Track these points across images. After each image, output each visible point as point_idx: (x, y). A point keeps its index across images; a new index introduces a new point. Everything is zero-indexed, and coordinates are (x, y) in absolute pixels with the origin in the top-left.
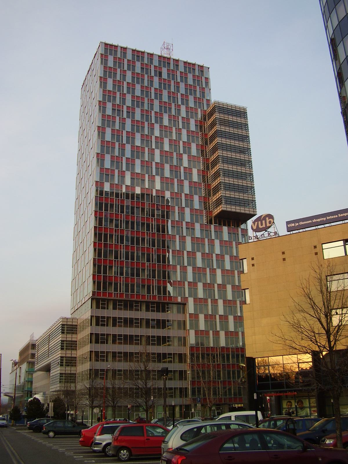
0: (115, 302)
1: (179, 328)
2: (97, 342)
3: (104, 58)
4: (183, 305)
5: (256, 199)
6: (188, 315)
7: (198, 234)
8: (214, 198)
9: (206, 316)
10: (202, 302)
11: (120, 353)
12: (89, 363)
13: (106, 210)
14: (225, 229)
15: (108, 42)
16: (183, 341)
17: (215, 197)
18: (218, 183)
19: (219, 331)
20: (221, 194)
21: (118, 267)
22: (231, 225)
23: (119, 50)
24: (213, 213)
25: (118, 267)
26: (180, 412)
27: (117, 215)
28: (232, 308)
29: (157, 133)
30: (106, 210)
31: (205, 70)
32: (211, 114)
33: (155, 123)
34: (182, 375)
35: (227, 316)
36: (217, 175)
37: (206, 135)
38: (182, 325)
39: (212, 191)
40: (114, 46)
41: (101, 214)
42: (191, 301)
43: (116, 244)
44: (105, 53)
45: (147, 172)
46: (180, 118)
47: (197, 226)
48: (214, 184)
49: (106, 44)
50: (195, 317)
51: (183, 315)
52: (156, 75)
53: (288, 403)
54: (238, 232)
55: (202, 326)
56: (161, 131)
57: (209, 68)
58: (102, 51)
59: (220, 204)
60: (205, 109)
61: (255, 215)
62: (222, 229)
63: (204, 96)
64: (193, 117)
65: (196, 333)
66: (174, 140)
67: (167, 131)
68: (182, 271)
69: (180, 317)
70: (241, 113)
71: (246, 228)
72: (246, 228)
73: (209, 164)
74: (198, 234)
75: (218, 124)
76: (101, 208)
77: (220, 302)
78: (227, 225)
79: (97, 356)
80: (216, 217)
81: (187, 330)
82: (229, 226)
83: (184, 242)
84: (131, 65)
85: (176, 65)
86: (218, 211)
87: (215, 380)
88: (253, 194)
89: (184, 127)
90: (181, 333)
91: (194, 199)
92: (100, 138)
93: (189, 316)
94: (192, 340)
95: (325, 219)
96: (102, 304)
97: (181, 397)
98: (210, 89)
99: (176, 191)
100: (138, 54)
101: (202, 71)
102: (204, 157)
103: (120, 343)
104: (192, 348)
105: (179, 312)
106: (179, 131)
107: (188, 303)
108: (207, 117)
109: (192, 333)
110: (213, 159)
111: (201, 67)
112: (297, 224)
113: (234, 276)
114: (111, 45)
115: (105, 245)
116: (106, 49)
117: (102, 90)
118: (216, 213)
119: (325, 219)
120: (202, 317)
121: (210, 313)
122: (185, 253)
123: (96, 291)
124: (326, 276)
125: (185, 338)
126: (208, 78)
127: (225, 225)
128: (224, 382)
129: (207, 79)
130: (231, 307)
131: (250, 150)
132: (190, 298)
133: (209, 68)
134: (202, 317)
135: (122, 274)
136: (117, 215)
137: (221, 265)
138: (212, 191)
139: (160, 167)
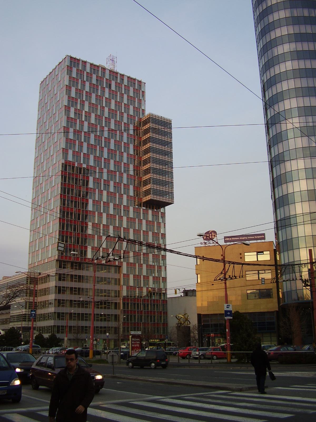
0: (72, 263)
1: (116, 284)
2: (59, 292)
3: (70, 69)
4: (119, 268)
5: (173, 161)
6: (122, 275)
7: (131, 215)
8: (144, 189)
9: (134, 276)
10: (132, 289)
11: (76, 288)
12: (54, 295)
13: (68, 193)
14: (150, 212)
15: (74, 56)
16: (118, 294)
17: (145, 187)
18: (148, 157)
19: (142, 264)
20: (150, 146)
21: (77, 190)
22: (154, 208)
23: (81, 62)
24: (142, 200)
25: (77, 190)
26: (114, 345)
27: (76, 198)
28: (152, 270)
29: (107, 95)
30: (68, 193)
31: (142, 85)
32: (146, 122)
33: (106, 87)
34: (116, 317)
35: (148, 277)
36: (146, 132)
37: (141, 158)
38: (117, 282)
39: (142, 123)
40: (77, 59)
41: (65, 196)
42: (125, 265)
43: (74, 245)
44: (70, 65)
45: (97, 210)
46: (123, 123)
47: (131, 209)
48: (144, 138)
49: (71, 58)
50: (127, 276)
51: (119, 274)
52: (106, 87)
53: (219, 340)
54: (159, 214)
55: (131, 283)
56: (109, 93)
57: (145, 83)
58: (67, 63)
59: (149, 132)
60: (141, 117)
61: (172, 204)
62: (148, 212)
63: (140, 88)
64: (132, 104)
65: (128, 288)
66: (118, 161)
67: (114, 76)
68: (120, 219)
69: (117, 276)
70: (167, 124)
71: (164, 233)
72: (165, 255)
73: (141, 161)
74: (131, 215)
75: (150, 122)
76: (65, 193)
77: (144, 266)
78: (151, 208)
79: (59, 303)
80: (144, 203)
81: (121, 286)
82: (153, 209)
83: (122, 156)
84: (89, 75)
85: (122, 79)
86: (147, 199)
87: (138, 322)
88: (172, 188)
89: (125, 151)
90: (117, 288)
91: (130, 277)
92: (65, 136)
93: (123, 276)
94: (124, 293)
95: (247, 238)
96: (63, 265)
97: (115, 321)
98: (145, 101)
99: (118, 203)
100: (94, 67)
101: (140, 86)
102: (138, 135)
103: (76, 269)
104: (124, 298)
105: (115, 272)
106: (122, 95)
107: (123, 266)
108: (142, 124)
109: (125, 288)
110: (145, 119)
111: (140, 82)
112: (231, 239)
113: (154, 226)
114: (75, 59)
115: (67, 221)
116: (71, 62)
117: (68, 76)
118: (145, 200)
119: (247, 238)
120: (131, 277)
121: (137, 274)
122: (122, 229)
123: (61, 230)
124: (246, 271)
125: (119, 291)
126: (144, 92)
127: (150, 208)
128: (144, 324)
129: (143, 92)
130: (151, 270)
131: (172, 125)
132: (125, 262)
133: (145, 83)
134: (131, 277)
135: (80, 196)
136: (76, 198)
137: (146, 261)
138: (142, 123)
139: (107, 184)
